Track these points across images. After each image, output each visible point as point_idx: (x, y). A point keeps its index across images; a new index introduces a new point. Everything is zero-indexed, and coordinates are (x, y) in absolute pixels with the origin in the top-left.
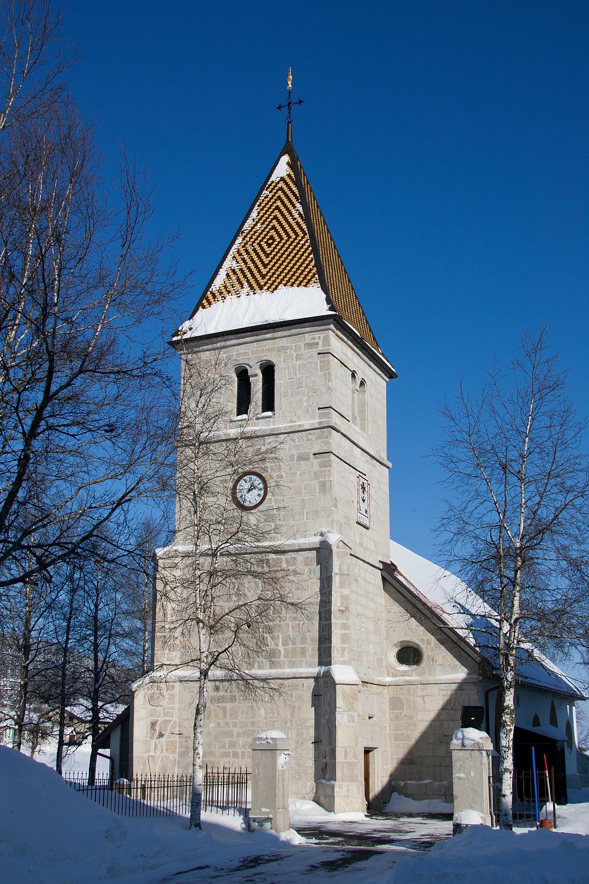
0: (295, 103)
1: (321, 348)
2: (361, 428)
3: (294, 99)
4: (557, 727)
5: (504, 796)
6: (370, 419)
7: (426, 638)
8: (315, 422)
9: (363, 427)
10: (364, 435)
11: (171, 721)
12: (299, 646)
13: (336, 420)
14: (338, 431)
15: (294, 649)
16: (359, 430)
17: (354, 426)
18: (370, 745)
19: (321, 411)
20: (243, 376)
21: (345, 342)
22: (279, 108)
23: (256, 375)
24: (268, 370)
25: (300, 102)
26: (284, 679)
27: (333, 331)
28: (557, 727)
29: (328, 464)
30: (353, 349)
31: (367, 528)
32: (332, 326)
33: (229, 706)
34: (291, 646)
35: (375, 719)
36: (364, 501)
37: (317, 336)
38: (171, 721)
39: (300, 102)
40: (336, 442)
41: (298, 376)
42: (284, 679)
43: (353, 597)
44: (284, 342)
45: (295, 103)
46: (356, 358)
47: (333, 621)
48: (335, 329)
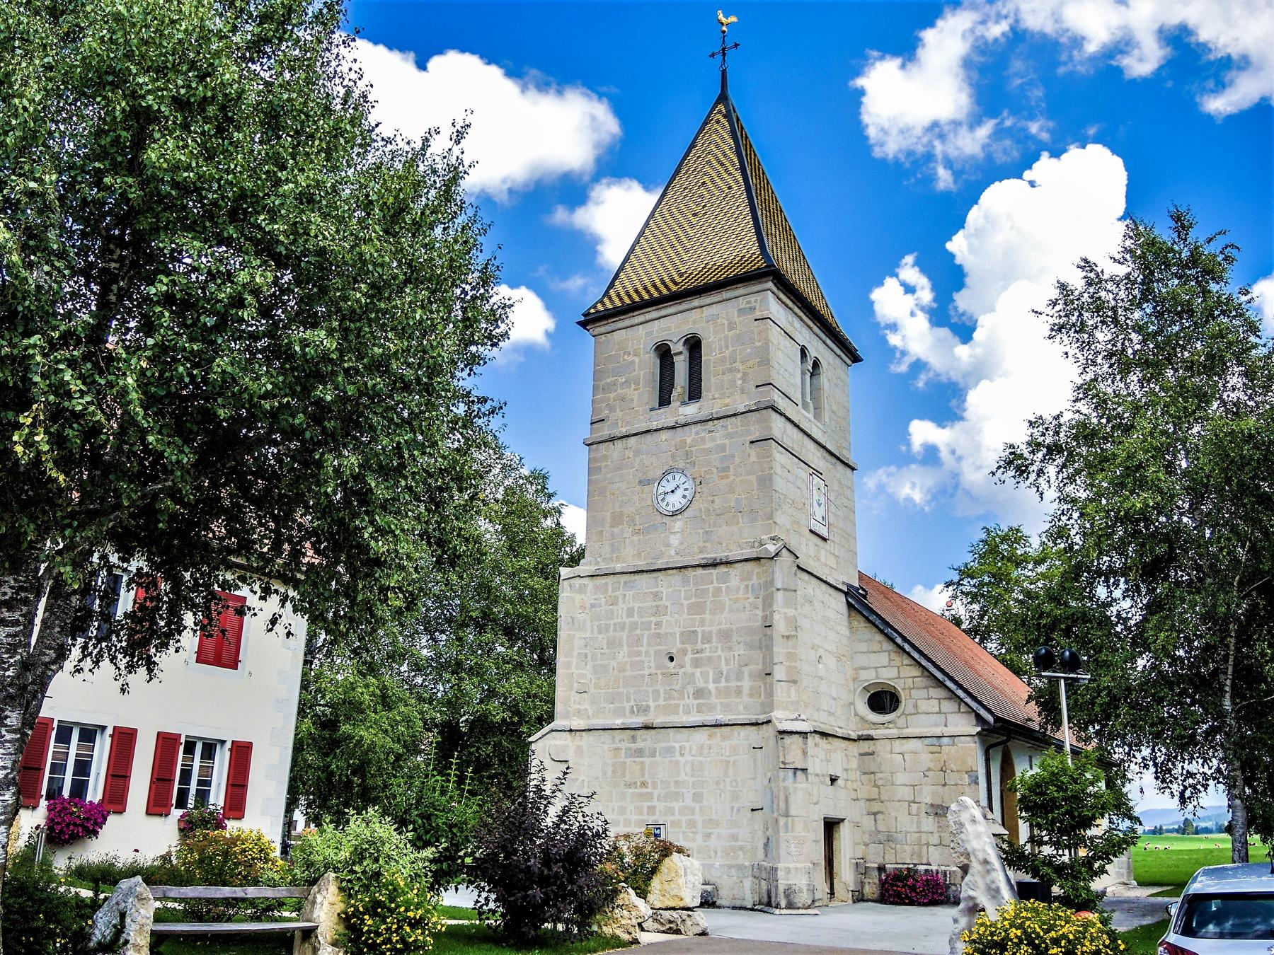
0: (730, 48)
1: (758, 314)
2: (815, 417)
3: (729, 43)
4: (578, 323)
5: (894, 327)
6: (827, 406)
7: (637, 605)
8: (750, 403)
9: (817, 416)
10: (819, 424)
11: (577, 779)
12: (734, 684)
13: (782, 404)
14: (782, 414)
15: (727, 688)
16: (812, 419)
17: (804, 412)
18: (833, 814)
19: (760, 389)
20: (664, 353)
21: (790, 308)
22: (713, 55)
23: (680, 353)
24: (694, 345)
25: (736, 45)
26: (634, 729)
27: (773, 293)
28: (578, 323)
29: (769, 456)
30: (802, 320)
31: (825, 540)
32: (770, 285)
33: (647, 760)
34: (723, 684)
35: (839, 782)
36: (820, 505)
37: (753, 300)
38: (577, 779)
39: (736, 45)
40: (778, 426)
41: (731, 349)
42: (634, 729)
43: (804, 623)
44: (715, 309)
45: (730, 48)
46: (806, 331)
47: (775, 649)
48: (775, 289)
